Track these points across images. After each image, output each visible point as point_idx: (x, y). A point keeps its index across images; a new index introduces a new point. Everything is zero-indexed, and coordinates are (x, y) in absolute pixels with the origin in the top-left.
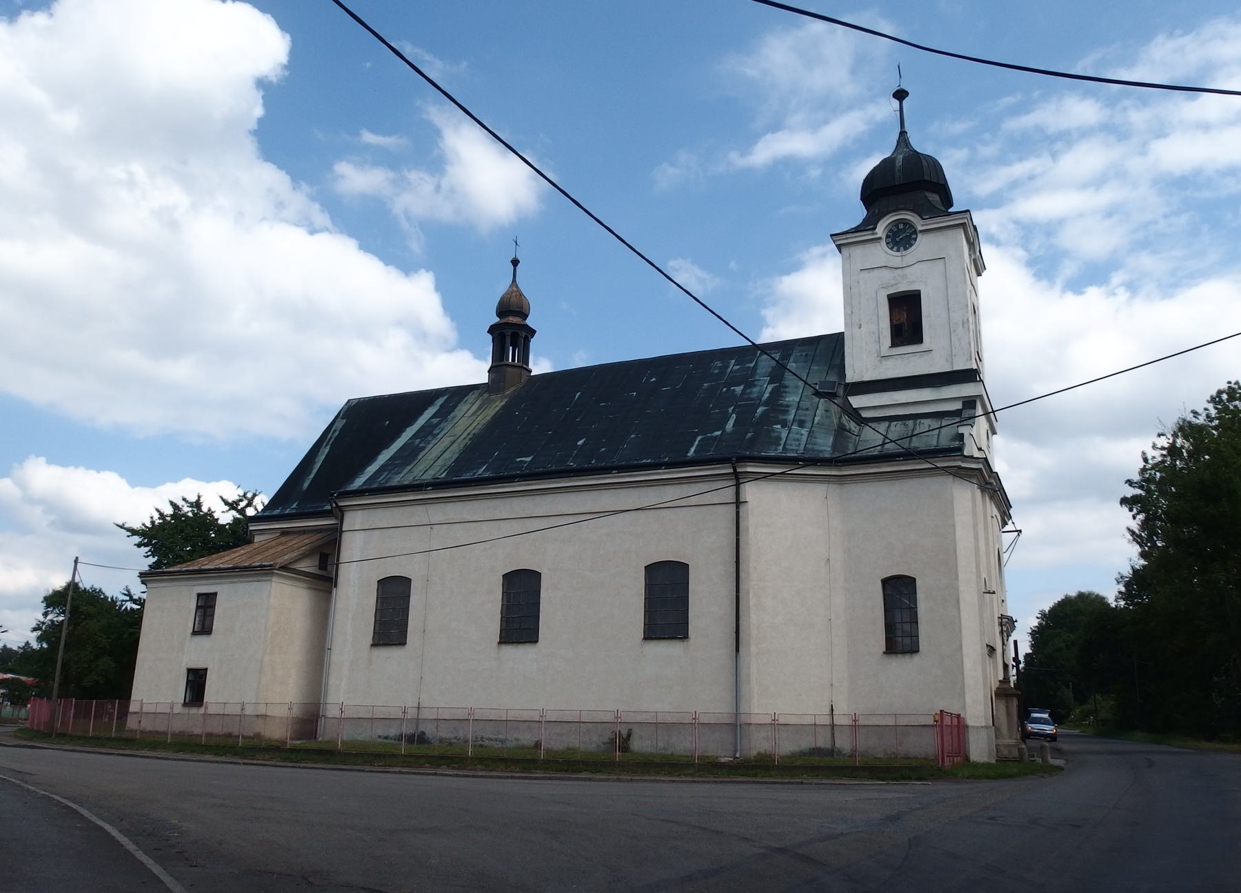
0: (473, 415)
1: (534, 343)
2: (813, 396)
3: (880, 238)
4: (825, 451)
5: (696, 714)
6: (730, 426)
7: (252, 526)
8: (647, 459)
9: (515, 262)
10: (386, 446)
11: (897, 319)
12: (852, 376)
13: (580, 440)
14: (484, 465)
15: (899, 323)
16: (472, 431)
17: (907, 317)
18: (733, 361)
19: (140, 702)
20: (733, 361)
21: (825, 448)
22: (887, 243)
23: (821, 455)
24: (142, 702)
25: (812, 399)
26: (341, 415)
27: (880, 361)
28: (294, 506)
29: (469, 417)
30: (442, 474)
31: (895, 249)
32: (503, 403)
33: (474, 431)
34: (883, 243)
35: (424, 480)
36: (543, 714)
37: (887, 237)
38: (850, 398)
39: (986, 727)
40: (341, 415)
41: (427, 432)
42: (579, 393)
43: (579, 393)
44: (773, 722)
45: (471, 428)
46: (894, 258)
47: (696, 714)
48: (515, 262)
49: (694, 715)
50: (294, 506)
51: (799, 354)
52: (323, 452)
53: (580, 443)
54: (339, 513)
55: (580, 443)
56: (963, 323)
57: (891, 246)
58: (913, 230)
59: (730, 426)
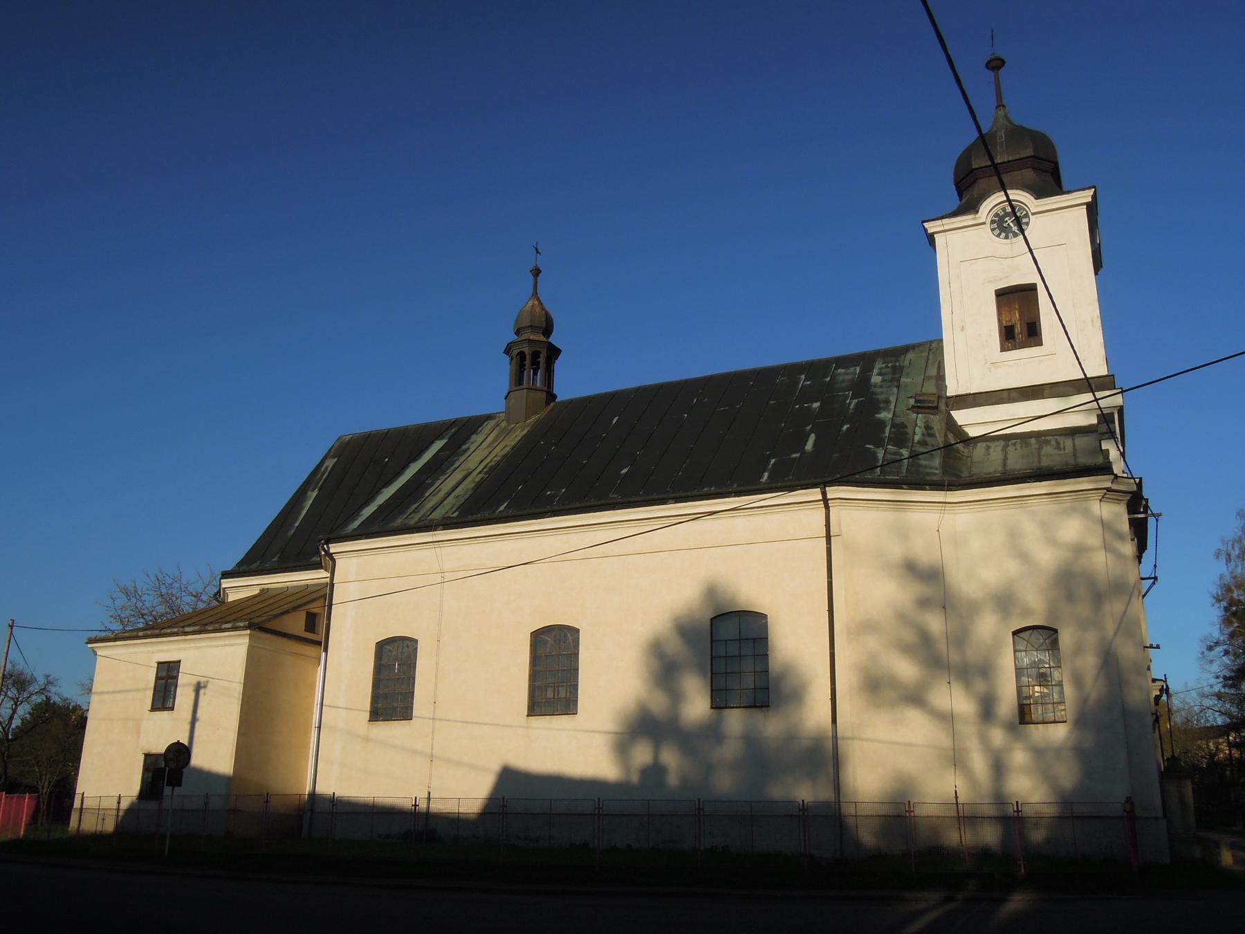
0: (487, 447)
1: (559, 365)
2: (908, 411)
3: (984, 223)
4: (936, 474)
5: (699, 804)
6: (809, 446)
7: (226, 582)
8: (819, 422)
9: (537, 272)
10: (388, 483)
11: (1007, 319)
12: (952, 389)
13: (623, 469)
14: (505, 502)
15: (1010, 324)
16: (488, 463)
17: (1020, 315)
18: (803, 376)
19: (81, 795)
20: (803, 376)
21: (933, 471)
22: (993, 230)
23: (928, 478)
24: (83, 795)
25: (908, 414)
26: (331, 454)
27: (990, 369)
28: (275, 559)
29: (485, 448)
30: (454, 513)
31: (1003, 235)
32: (525, 432)
33: (495, 459)
34: (988, 227)
35: (434, 520)
36: (599, 804)
37: (993, 222)
38: (954, 414)
39: (954, 817)
40: (331, 454)
41: (437, 468)
42: (617, 418)
43: (617, 418)
44: (801, 813)
45: (488, 460)
46: (1002, 246)
47: (699, 804)
48: (537, 272)
49: (907, 806)
50: (275, 559)
51: (884, 365)
52: (310, 497)
53: (624, 471)
54: (329, 563)
55: (624, 471)
56: (1092, 321)
57: (997, 232)
58: (1025, 212)
59: (809, 446)
